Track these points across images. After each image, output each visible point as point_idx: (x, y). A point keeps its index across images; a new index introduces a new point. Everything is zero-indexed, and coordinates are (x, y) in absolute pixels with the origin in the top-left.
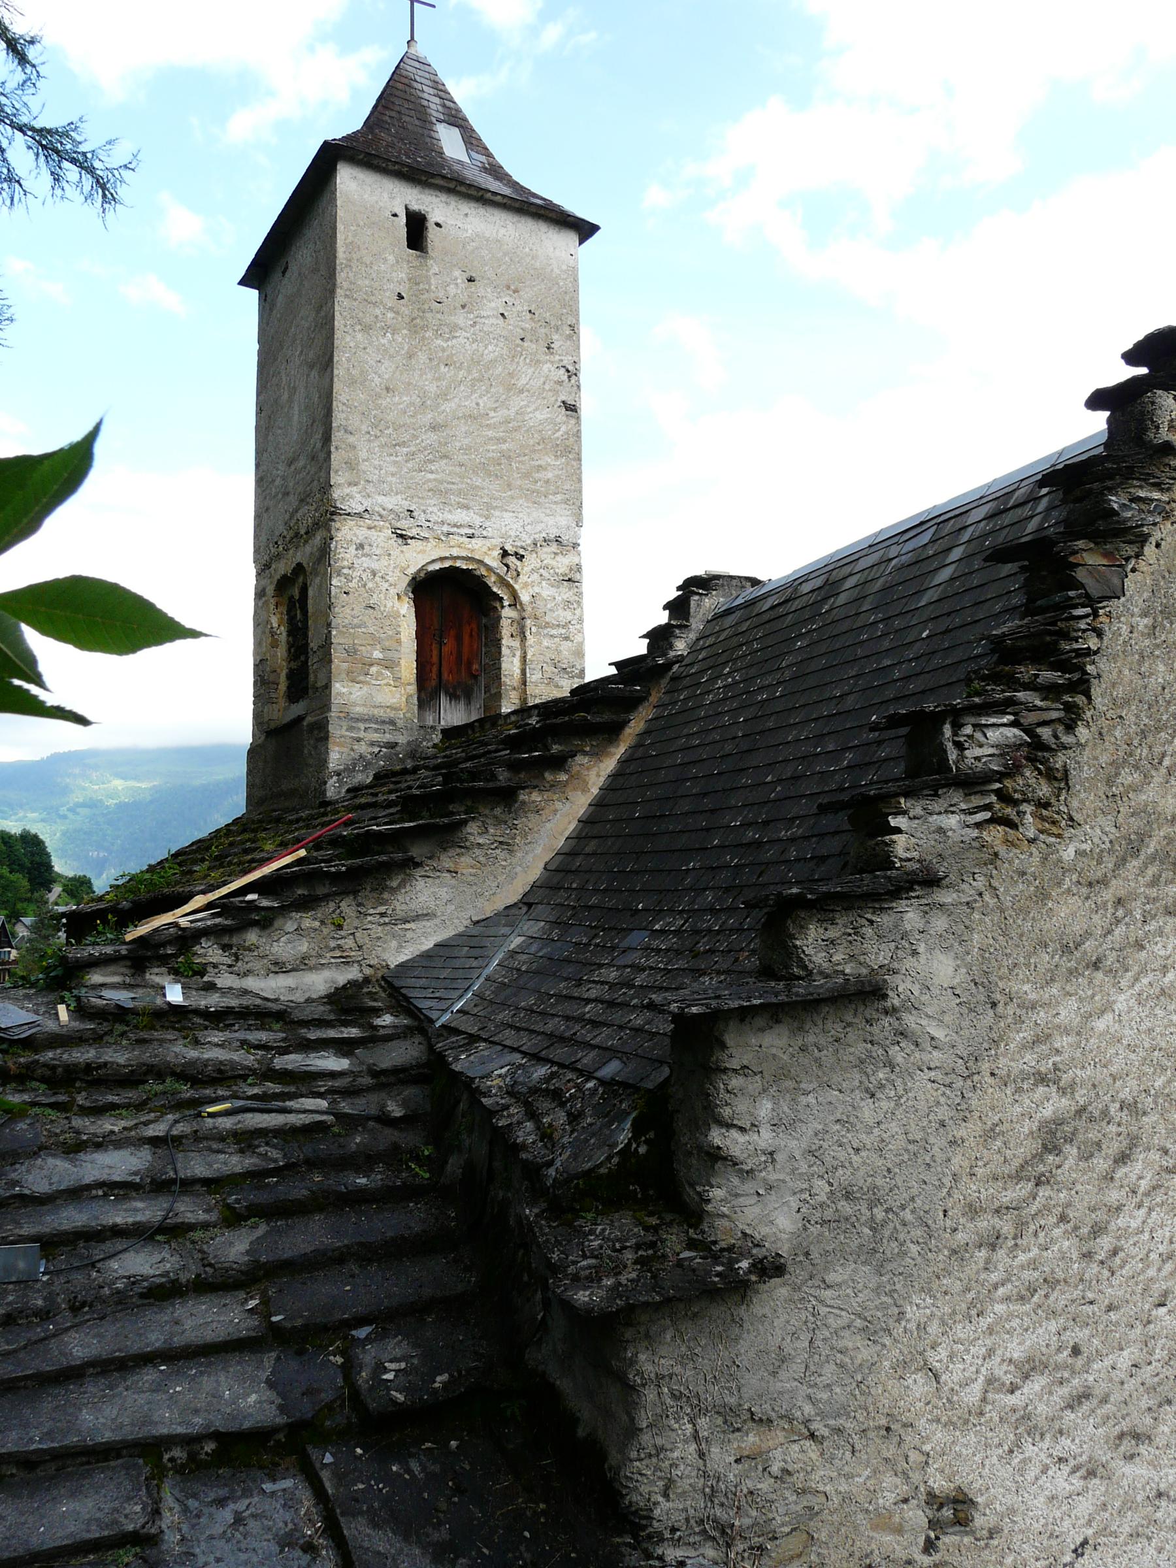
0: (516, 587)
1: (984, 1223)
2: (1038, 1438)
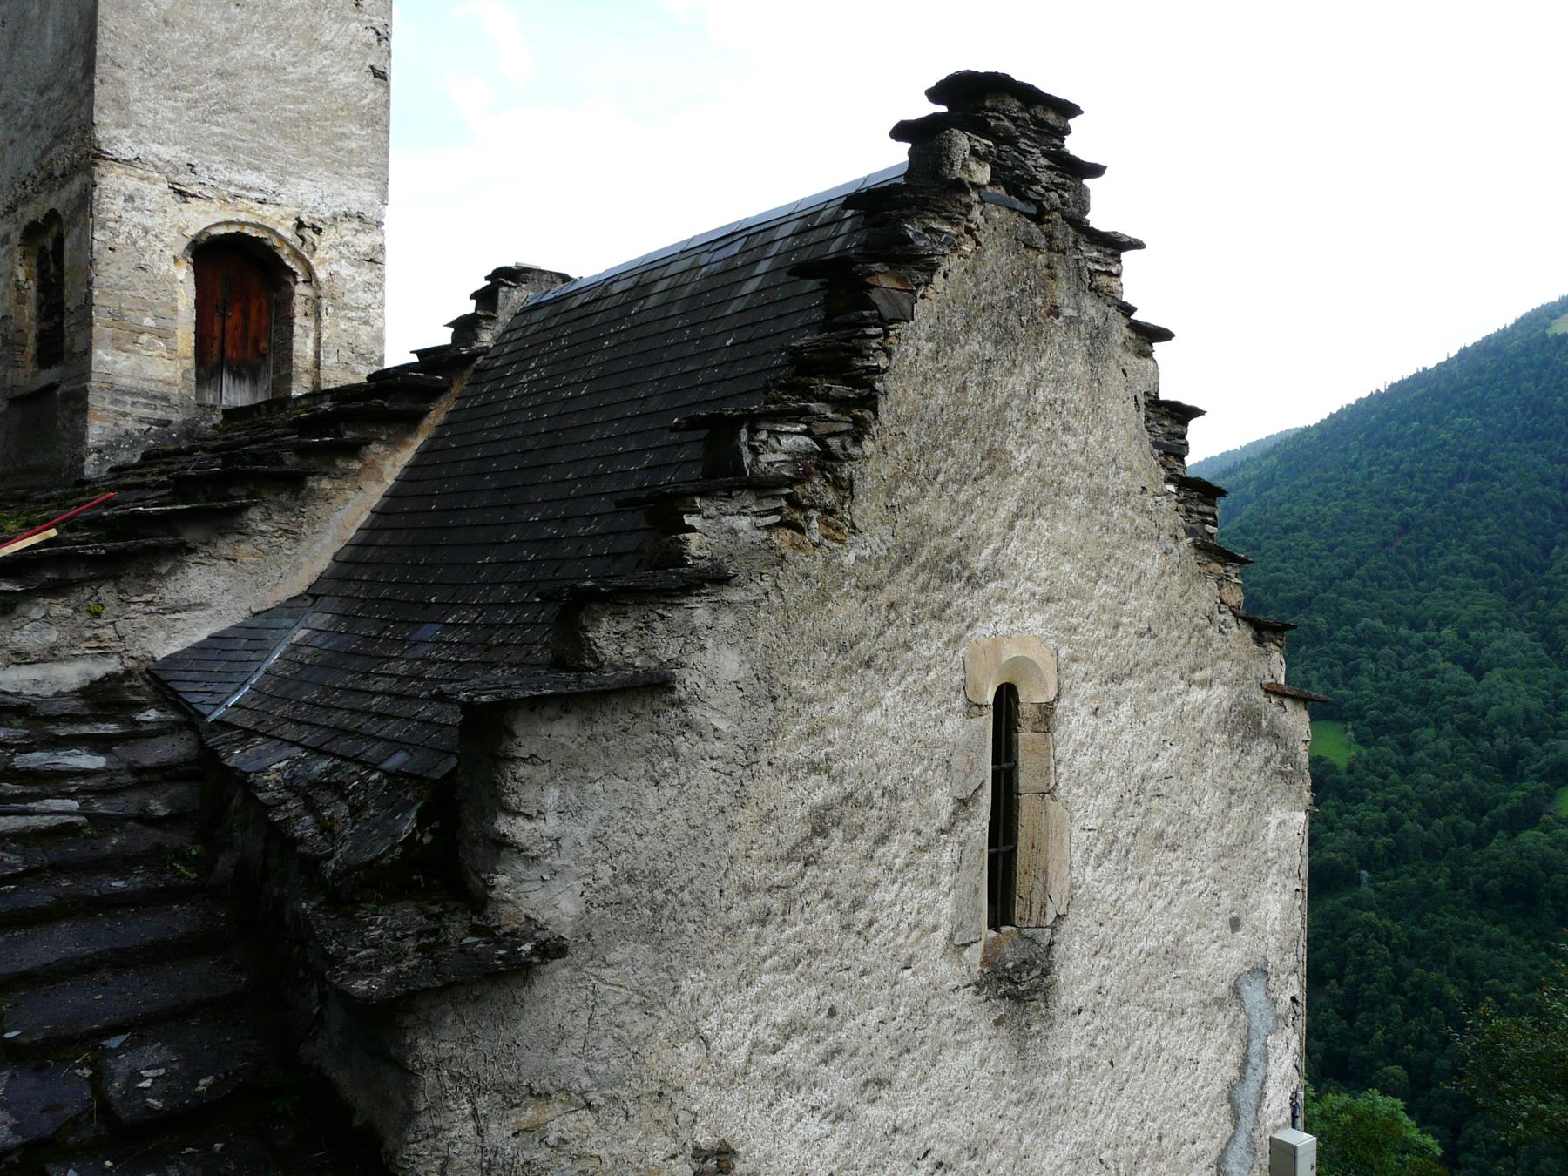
0: (313, 262)
1: (756, 902)
2: (795, 1091)
